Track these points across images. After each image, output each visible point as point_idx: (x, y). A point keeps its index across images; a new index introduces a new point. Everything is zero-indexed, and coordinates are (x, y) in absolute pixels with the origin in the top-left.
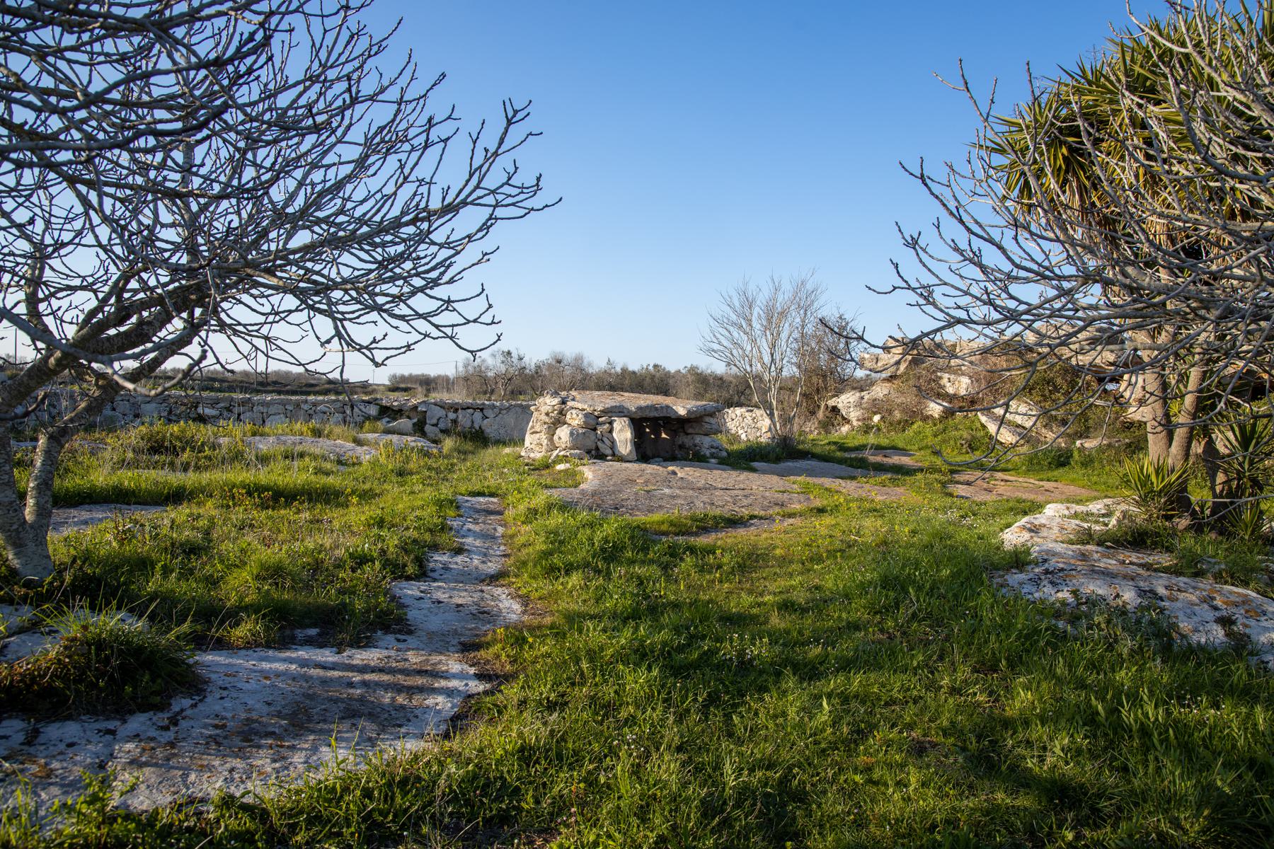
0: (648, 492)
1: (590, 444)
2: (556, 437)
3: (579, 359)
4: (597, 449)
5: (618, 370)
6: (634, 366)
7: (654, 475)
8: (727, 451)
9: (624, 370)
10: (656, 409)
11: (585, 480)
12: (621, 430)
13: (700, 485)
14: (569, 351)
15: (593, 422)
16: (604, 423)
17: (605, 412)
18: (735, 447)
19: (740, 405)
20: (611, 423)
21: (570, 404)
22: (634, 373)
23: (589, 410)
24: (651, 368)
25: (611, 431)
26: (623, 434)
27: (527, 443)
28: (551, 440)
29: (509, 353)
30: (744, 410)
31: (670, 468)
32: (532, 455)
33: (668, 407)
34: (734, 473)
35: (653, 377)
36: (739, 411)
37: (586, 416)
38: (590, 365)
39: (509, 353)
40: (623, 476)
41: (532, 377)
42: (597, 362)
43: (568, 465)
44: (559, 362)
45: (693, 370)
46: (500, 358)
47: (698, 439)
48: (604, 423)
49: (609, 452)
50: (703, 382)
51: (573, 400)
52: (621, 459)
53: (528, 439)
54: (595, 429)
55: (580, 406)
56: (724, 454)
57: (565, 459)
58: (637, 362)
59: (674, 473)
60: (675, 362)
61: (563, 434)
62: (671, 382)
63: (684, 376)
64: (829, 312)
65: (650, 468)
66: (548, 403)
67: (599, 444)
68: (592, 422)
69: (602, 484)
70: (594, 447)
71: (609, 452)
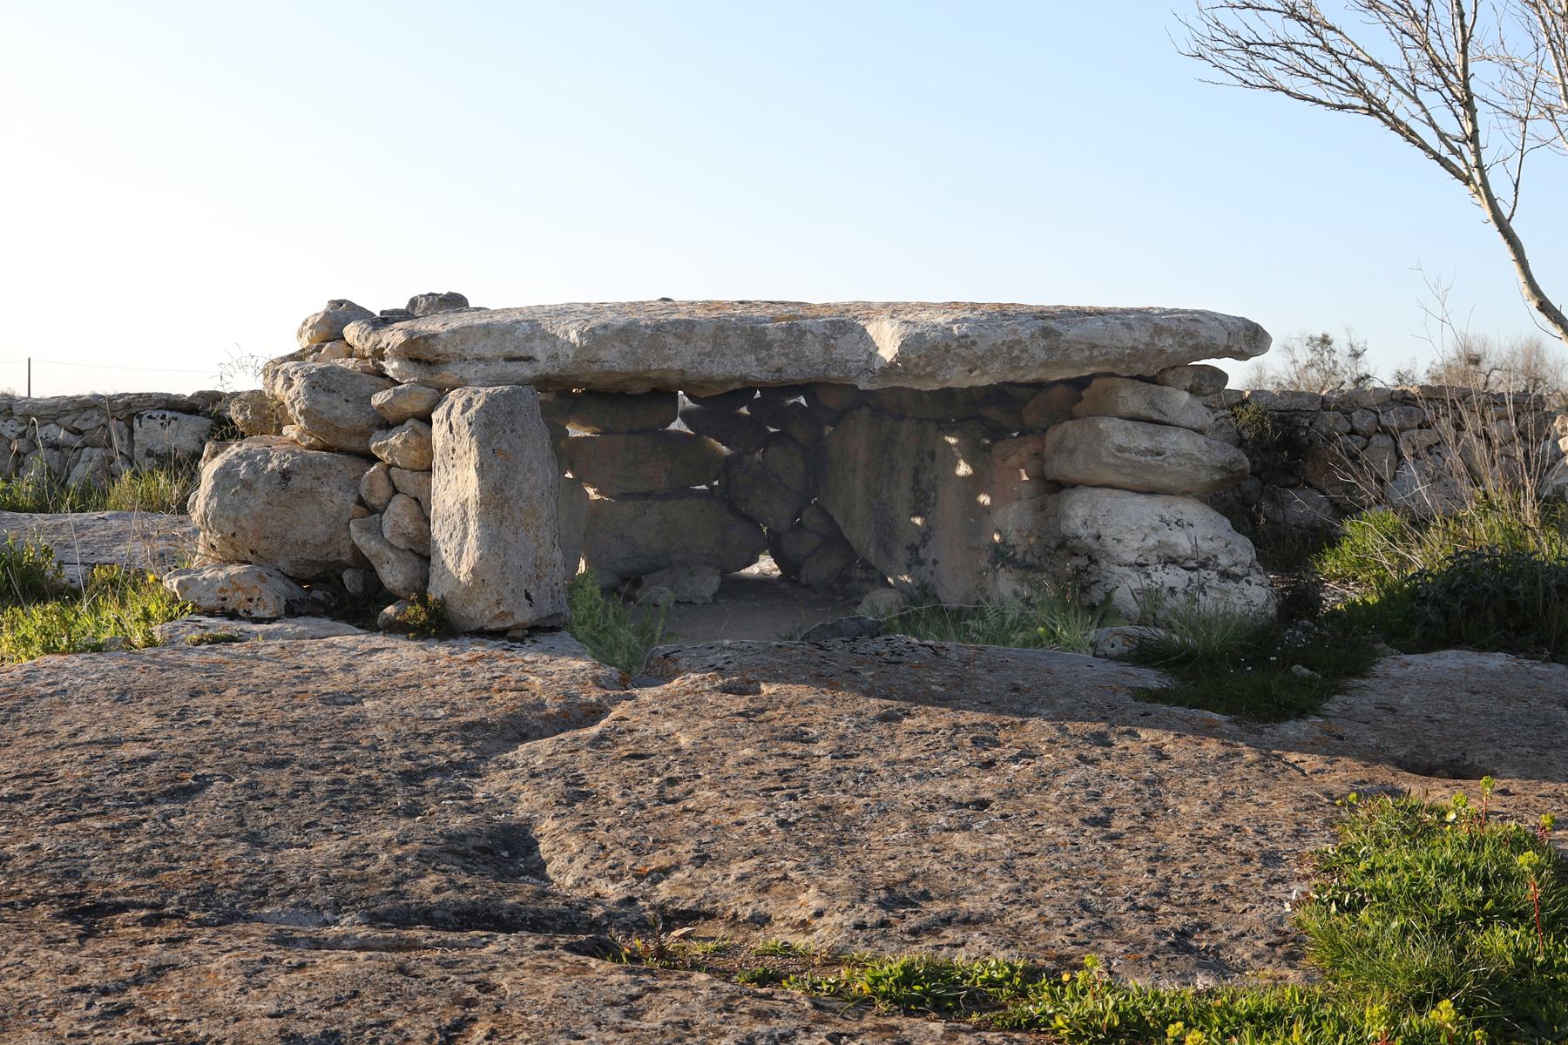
29: (1325, 341)
39: (1325, 341)
44: (1476, 361)
52: (440, 625)
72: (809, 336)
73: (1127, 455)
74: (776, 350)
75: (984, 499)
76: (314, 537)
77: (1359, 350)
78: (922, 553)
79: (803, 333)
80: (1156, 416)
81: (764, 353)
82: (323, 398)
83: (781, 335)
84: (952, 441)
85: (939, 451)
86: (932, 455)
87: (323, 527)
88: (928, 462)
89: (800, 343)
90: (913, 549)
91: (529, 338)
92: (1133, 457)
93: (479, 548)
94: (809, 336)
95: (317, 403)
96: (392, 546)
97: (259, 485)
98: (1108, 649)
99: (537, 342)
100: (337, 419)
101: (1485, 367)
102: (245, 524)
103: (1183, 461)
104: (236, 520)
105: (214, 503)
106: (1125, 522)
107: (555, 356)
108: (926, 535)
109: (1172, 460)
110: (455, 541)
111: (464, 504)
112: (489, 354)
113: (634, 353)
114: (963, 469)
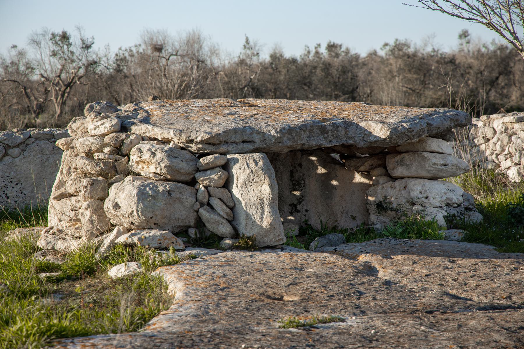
0: (308, 328)
1: (183, 213)
2: (108, 205)
3: (193, 42)
4: (200, 223)
5: (265, 57)
6: (293, 51)
7: (325, 279)
8: (480, 208)
9: (276, 58)
10: (323, 130)
11: (164, 302)
12: (248, 182)
13: (429, 298)
14: (175, 32)
15: (185, 167)
16: (210, 168)
17: (213, 143)
18: (499, 198)
19: (492, 109)
20: (226, 167)
21: (138, 129)
22: (294, 61)
23: (177, 141)
24: (323, 50)
25: (227, 184)
26: (252, 188)
27: (52, 219)
28: (98, 209)
29: (65, 37)
30: (509, 118)
31: (363, 258)
32: (60, 245)
33: (348, 124)
34: (506, 264)
35: (327, 67)
36: (499, 121)
37: (171, 154)
38: (214, 52)
39: (65, 37)
40: (253, 288)
41: (111, 77)
42: (226, 49)
43: (133, 265)
44: (159, 49)
45: (399, 49)
46: (48, 47)
47: (417, 189)
48: (210, 168)
49: (225, 229)
50: (420, 70)
51: (146, 121)
52: (252, 245)
53: (57, 213)
54: (193, 183)
55: (158, 133)
56: (477, 217)
57: (130, 251)
58: (297, 42)
59: (370, 270)
60: (364, 41)
61: (124, 196)
62: (361, 74)
63: (383, 61)
64: (302, 163)
65: (317, 262)
66: (91, 129)
67: (204, 213)
68: (187, 168)
69: (202, 316)
70: (195, 225)
71: (225, 229)
72: (340, 128)
73: (436, 166)
74: (330, 134)
75: (335, 183)
76: (182, 216)
77: (89, 43)
78: (298, 207)
79: (338, 127)
80: (440, 151)
81: (326, 135)
82: (174, 160)
83: (331, 128)
84: (314, 158)
85: (304, 163)
86: (300, 165)
87: (184, 212)
88: (298, 168)
89: (337, 131)
90: (294, 206)
91: (251, 134)
92: (439, 167)
93: (272, 216)
94: (340, 128)
95: (173, 162)
96: (224, 218)
97: (160, 197)
98: (453, 238)
99: (255, 135)
100: (181, 169)
101: (164, 53)
102: (157, 213)
103: (453, 167)
104: (153, 212)
105: (141, 206)
106: (437, 191)
107: (264, 141)
108: (300, 200)
109: (450, 167)
110: (259, 214)
111: (262, 200)
112: (238, 141)
113: (293, 138)
114: (321, 170)
